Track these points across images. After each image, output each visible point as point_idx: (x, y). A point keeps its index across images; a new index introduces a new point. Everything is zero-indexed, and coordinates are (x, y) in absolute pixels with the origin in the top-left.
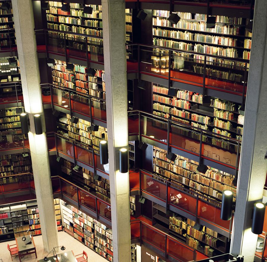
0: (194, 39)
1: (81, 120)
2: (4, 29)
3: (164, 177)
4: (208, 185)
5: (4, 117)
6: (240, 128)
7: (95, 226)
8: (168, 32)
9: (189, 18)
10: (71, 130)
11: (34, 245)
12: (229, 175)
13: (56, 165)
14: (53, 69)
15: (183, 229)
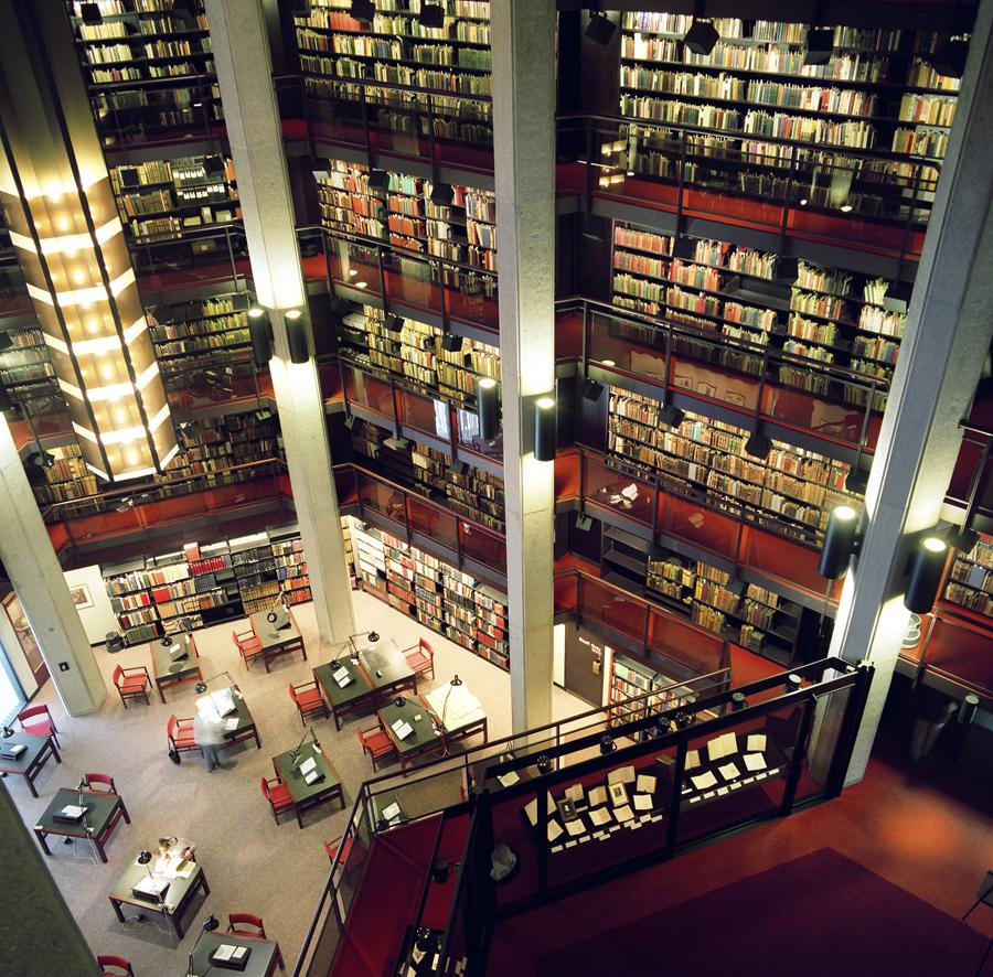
0: (745, 97)
1: (408, 322)
2: (181, 75)
3: (638, 462)
4: (760, 482)
5: (201, 320)
6: (862, 339)
7: (446, 578)
8: (666, 78)
9: (736, 36)
10: (377, 346)
11: (299, 631)
12: (821, 458)
13: (341, 434)
14: (321, 186)
15: (685, 587)
